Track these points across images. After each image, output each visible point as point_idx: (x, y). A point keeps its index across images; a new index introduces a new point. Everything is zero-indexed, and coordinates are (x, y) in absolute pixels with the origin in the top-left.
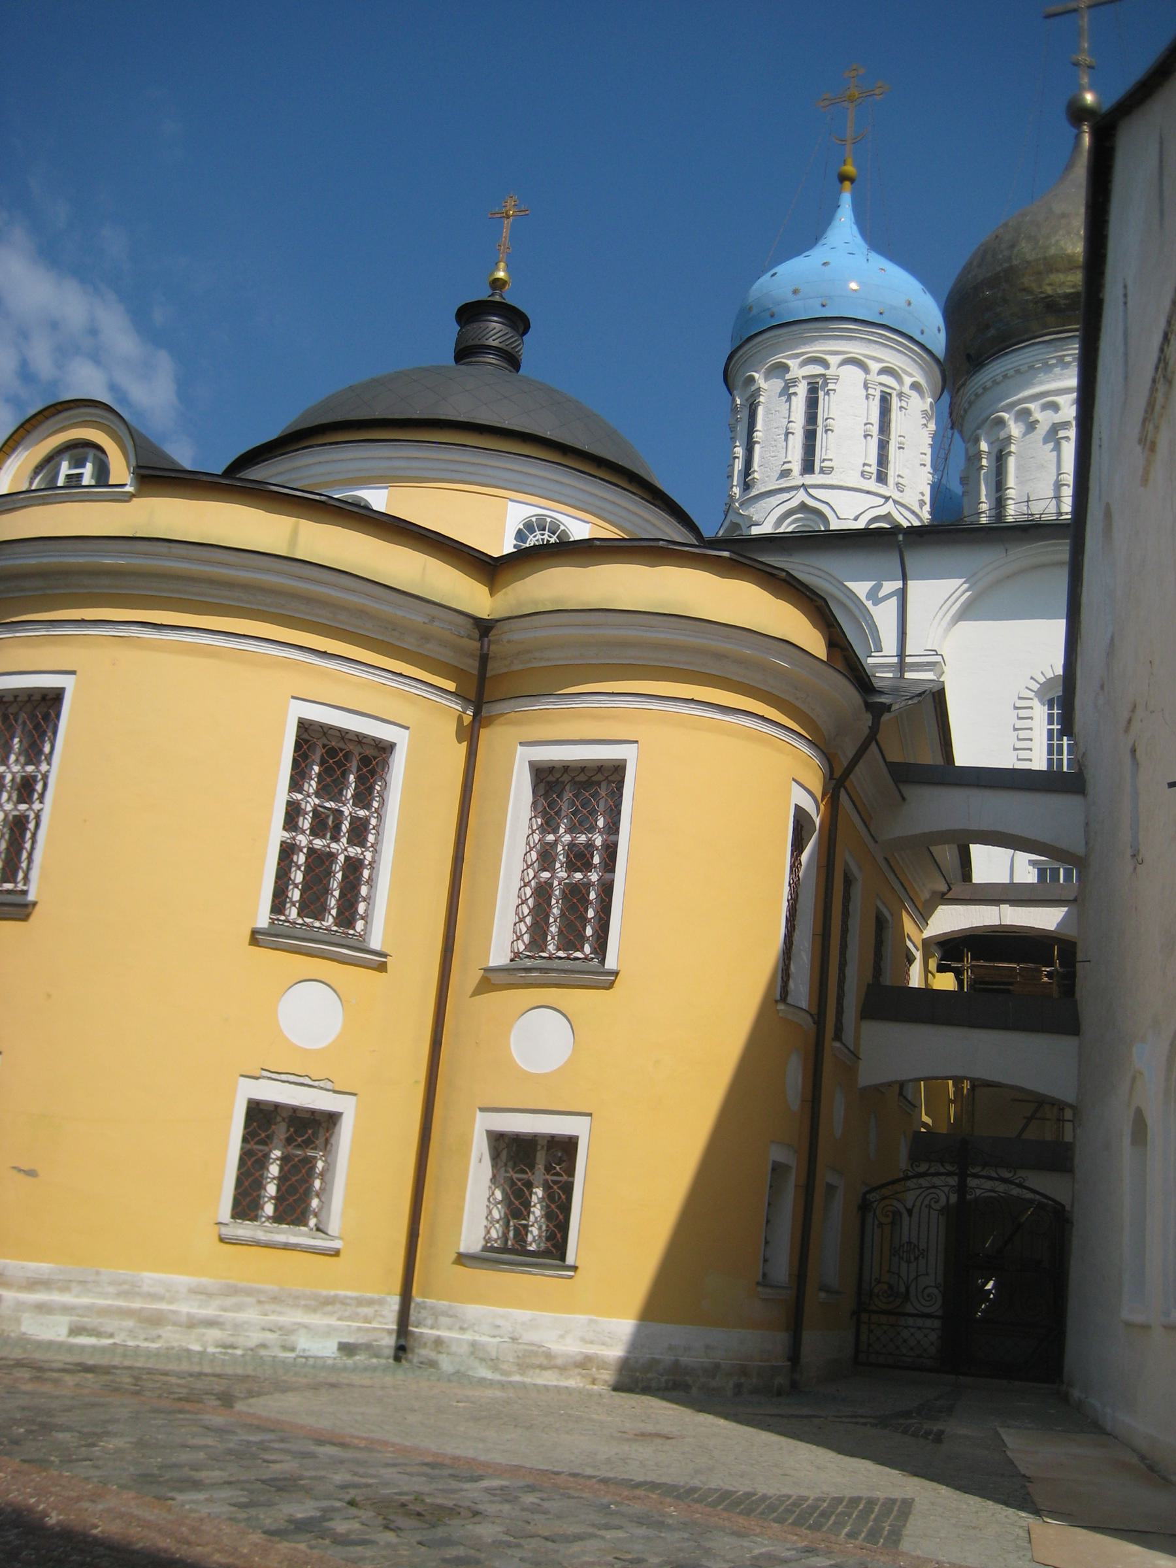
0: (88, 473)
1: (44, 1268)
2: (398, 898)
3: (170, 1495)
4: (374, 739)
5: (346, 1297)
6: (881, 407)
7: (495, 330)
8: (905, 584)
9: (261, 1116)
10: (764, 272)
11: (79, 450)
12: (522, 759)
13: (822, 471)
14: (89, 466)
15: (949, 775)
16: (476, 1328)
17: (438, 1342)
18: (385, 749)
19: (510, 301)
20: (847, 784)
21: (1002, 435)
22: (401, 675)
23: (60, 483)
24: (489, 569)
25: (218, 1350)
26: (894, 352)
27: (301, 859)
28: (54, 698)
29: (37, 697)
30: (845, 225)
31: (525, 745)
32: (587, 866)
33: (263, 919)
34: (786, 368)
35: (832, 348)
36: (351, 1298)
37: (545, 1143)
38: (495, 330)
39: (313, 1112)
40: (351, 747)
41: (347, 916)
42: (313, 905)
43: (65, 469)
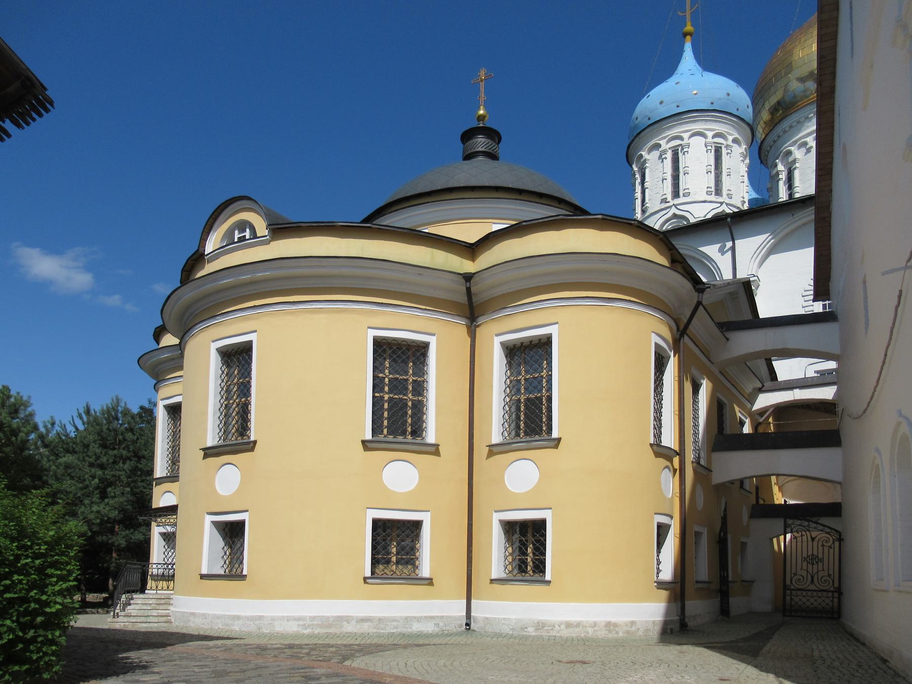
0: (247, 234)
2: (439, 419)
7: (481, 143)
8: (734, 243)
9: (379, 526)
10: (643, 97)
12: (497, 341)
13: (684, 196)
14: (248, 230)
15: (757, 323)
18: (425, 346)
19: (487, 125)
20: (688, 332)
21: (791, 159)
23: (236, 240)
24: (471, 250)
30: (688, 59)
31: (496, 335)
33: (368, 436)
34: (659, 146)
35: (683, 129)
38: (481, 143)
43: (237, 235)
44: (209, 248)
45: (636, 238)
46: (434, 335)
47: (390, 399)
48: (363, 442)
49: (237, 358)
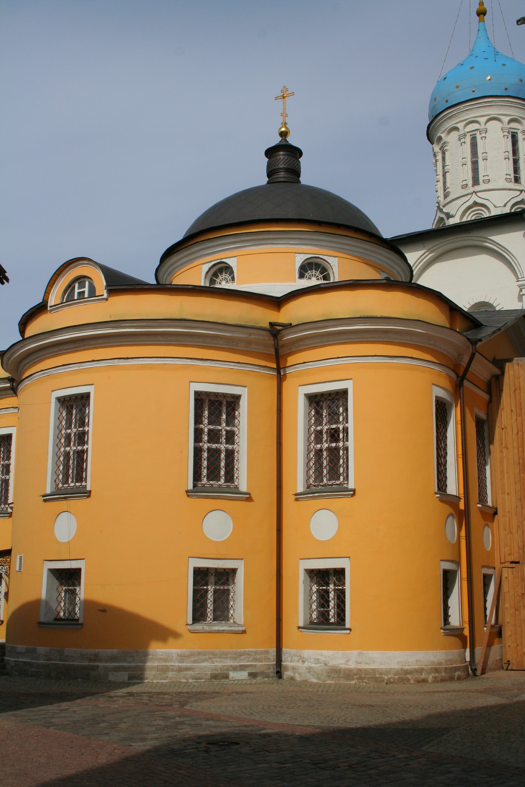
1: (115, 651)
3: (131, 744)
4: (231, 394)
5: (249, 651)
6: (512, 141)
9: (201, 575)
11: (80, 279)
16: (309, 660)
17: (294, 668)
18: (237, 398)
22: (239, 363)
24: (277, 303)
25: (194, 681)
26: (517, 109)
27: (205, 455)
28: (86, 397)
29: (80, 397)
32: (337, 440)
34: (456, 129)
35: (480, 113)
36: (252, 652)
37: (333, 572)
39: (225, 569)
40: (221, 399)
41: (230, 476)
42: (213, 475)
44: (52, 302)
45: (418, 297)
46: (246, 387)
47: (209, 449)
48: (187, 492)
49: (75, 406)
